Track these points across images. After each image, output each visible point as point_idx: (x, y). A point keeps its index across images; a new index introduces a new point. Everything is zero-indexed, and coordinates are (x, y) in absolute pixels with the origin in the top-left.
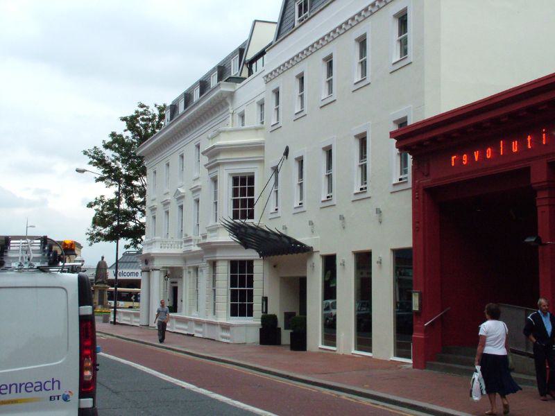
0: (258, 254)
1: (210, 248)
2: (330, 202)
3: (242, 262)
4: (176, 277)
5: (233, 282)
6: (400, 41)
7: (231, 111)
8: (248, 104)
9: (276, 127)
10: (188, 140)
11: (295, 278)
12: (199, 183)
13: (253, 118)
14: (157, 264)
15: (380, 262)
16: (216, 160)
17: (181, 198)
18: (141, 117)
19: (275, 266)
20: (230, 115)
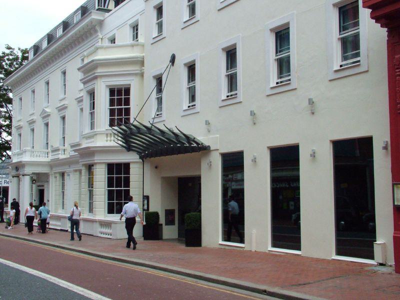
0: (138, 157)
1: (89, 152)
2: (194, 110)
3: (119, 165)
4: (42, 182)
5: (110, 183)
6: (158, 23)
7: (101, 37)
8: (118, 28)
9: (158, 39)
10: (74, 55)
11: (173, 178)
12: (34, 117)
13: (125, 36)
14: (28, 170)
15: (254, 161)
16: (95, 73)
17: (46, 116)
18: (7, 57)
19: (156, 167)
20: (100, 40)
